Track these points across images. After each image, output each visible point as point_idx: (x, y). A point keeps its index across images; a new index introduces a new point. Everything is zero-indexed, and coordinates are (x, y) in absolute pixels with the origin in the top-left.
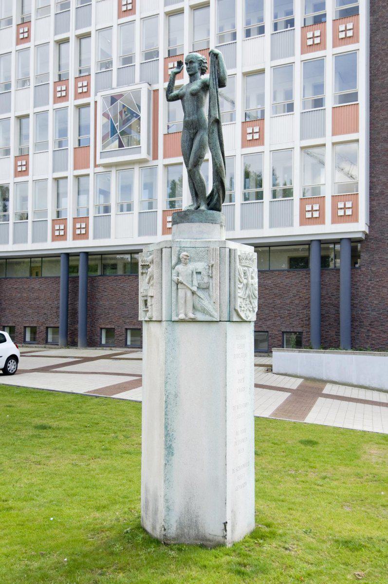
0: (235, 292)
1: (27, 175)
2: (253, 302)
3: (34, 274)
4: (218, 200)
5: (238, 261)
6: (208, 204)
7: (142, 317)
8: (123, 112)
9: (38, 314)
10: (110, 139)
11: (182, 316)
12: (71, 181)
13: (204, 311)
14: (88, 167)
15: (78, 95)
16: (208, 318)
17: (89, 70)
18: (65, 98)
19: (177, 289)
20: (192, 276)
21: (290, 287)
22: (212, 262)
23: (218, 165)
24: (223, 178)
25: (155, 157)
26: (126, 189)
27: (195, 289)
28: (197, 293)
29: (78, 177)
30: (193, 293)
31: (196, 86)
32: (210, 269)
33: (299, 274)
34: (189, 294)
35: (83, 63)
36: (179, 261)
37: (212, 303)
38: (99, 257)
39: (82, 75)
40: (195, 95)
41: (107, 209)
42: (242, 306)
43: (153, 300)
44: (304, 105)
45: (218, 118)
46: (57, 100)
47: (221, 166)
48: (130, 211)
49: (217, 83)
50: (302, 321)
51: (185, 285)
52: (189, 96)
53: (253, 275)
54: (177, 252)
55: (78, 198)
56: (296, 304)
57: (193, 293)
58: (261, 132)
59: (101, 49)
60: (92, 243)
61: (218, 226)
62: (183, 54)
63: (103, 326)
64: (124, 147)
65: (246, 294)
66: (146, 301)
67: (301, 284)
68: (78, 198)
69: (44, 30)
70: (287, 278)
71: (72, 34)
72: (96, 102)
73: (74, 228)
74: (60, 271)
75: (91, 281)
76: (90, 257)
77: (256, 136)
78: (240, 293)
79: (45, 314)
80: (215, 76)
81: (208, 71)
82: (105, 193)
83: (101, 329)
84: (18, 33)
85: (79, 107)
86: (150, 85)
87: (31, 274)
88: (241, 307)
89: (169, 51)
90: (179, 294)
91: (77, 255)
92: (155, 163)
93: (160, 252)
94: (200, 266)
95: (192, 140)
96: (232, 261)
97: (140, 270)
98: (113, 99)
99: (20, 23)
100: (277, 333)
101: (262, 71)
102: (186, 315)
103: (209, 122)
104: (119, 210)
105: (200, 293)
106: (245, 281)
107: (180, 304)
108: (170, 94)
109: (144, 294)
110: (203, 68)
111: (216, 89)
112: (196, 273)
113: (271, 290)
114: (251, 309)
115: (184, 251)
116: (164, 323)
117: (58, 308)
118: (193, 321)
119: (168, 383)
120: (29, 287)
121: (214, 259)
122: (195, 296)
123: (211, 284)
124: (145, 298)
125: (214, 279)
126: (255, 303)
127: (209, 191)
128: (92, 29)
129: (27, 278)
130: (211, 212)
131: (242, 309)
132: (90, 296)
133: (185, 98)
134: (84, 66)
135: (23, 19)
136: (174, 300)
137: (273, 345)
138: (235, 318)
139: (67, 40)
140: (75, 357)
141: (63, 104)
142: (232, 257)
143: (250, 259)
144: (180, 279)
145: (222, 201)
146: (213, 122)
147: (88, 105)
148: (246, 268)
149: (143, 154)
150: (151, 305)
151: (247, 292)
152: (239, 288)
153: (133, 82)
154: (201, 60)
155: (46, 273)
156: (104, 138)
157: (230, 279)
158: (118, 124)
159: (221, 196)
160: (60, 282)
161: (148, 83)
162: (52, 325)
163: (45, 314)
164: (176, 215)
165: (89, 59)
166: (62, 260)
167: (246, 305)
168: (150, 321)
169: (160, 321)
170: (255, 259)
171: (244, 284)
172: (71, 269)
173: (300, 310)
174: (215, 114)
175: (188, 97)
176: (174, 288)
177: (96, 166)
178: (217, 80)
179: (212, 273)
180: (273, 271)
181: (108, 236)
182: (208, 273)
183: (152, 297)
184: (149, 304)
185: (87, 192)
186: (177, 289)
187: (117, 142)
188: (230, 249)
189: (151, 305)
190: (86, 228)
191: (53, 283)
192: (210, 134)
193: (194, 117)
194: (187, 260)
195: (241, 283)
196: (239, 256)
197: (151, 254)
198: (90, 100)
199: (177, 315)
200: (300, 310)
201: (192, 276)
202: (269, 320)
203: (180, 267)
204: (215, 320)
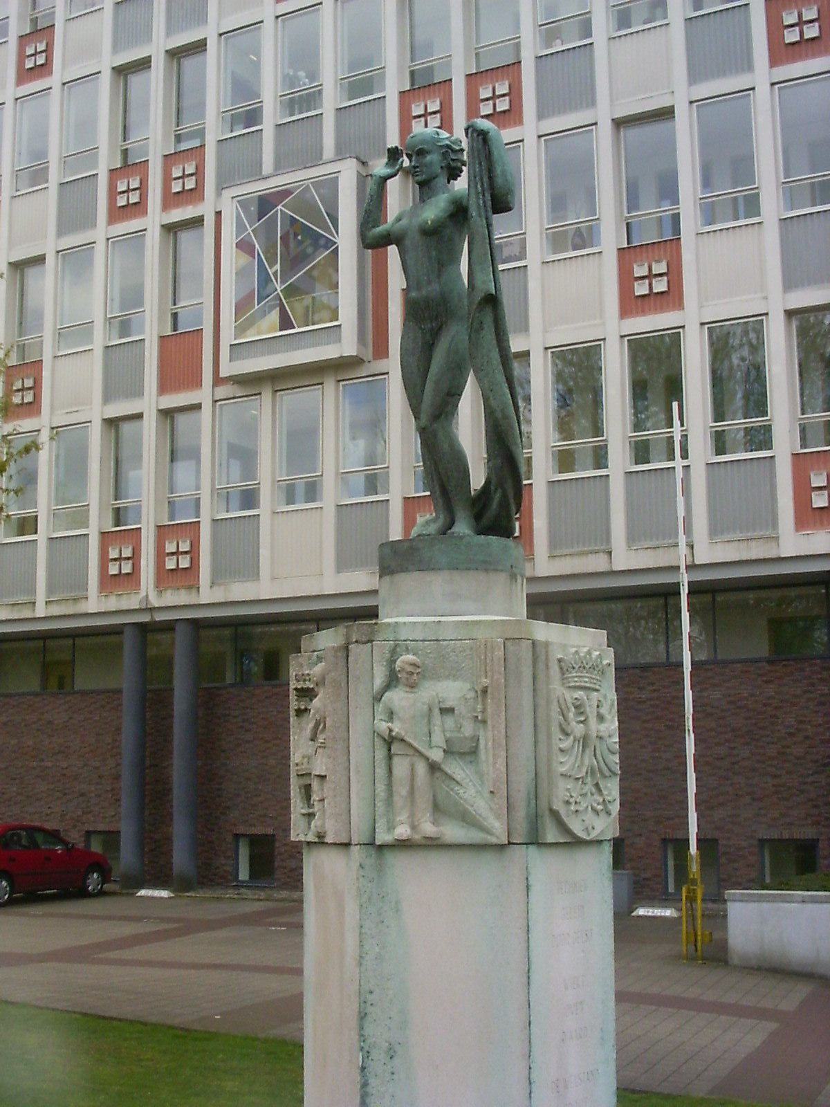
0: (549, 761)
1: (38, 412)
2: (606, 787)
3: (53, 682)
4: (504, 505)
5: (555, 669)
6: (478, 517)
7: (299, 832)
8: (292, 236)
9: (65, 794)
10: (256, 307)
11: (402, 831)
12: (150, 424)
13: (466, 818)
14: (196, 383)
15: (171, 200)
16: (475, 836)
17: (201, 133)
18: (138, 208)
19: (390, 757)
20: (429, 722)
21: (776, 708)
22: (485, 681)
23: (499, 415)
24: (513, 448)
25: (381, 351)
26: (302, 445)
27: (436, 755)
28: (443, 766)
29: (168, 414)
30: (434, 767)
31: (434, 211)
32: (480, 699)
33: (802, 670)
34: (421, 768)
35: (185, 115)
36: (392, 680)
37: (487, 795)
38: (227, 632)
39: (184, 146)
40: (431, 233)
41: (249, 498)
42: (572, 800)
43: (328, 785)
44: (791, 194)
45: (494, 292)
46: (118, 213)
47: (506, 417)
48: (313, 500)
49: (489, 203)
50: (816, 806)
51: (410, 745)
52: (417, 236)
53: (603, 711)
54: (388, 655)
55: (171, 470)
56: (798, 758)
57: (434, 767)
58: (674, 274)
59: (233, 73)
60: (211, 594)
61: (502, 578)
62: (451, 80)
63: (241, 829)
64: (294, 328)
65: (582, 763)
66: (307, 789)
67: (809, 700)
68: (171, 470)
69: (87, 45)
70: (767, 682)
71: (157, 47)
72: (218, 214)
73: (161, 555)
74: (125, 677)
75: (208, 702)
76: (203, 633)
77: (660, 286)
78: (565, 764)
79: (82, 795)
80: (482, 185)
81: (465, 174)
82: (245, 456)
83: (237, 836)
84: (22, 57)
85: (171, 230)
86: (363, 163)
87: (44, 686)
88: (568, 803)
89: (412, 73)
90: (396, 771)
91: (169, 627)
92: (380, 365)
93: (341, 654)
94: (452, 690)
95: (429, 348)
96: (541, 676)
97: (294, 703)
98: (265, 204)
99: (28, 32)
100: (744, 844)
101: (666, 114)
102: (414, 827)
103: (470, 303)
104: (283, 497)
105: (456, 769)
106: (579, 730)
107: (396, 798)
108: (370, 229)
109: (304, 768)
110: (453, 164)
111: (487, 219)
112: (441, 710)
113: (724, 718)
114: (600, 807)
115: (407, 651)
116: (355, 850)
117: (117, 778)
118: (433, 845)
119: (369, 1018)
120: (40, 720)
121: (489, 674)
122: (438, 774)
123: (482, 742)
124: (306, 781)
125: (490, 728)
126: (612, 789)
127: (477, 480)
128: (209, 31)
129: (36, 695)
130: (482, 538)
131: (573, 808)
132: (207, 743)
133: (407, 242)
134: (188, 126)
135: (34, 21)
136: (381, 788)
137: (734, 880)
138: (551, 835)
139: (144, 64)
140: (169, 920)
141: (133, 225)
142: (541, 666)
143: (593, 668)
144: (397, 728)
145: (513, 508)
146: (480, 303)
147: (198, 222)
148: (581, 693)
149: (348, 346)
150: (322, 800)
151: (587, 762)
152: (562, 750)
153: (315, 158)
154: (448, 146)
155: (84, 680)
156: (241, 307)
157: (535, 726)
158: (278, 267)
159: (511, 493)
160: (121, 705)
161: (358, 159)
162: (101, 827)
163: (82, 795)
164: (387, 551)
165: (202, 105)
166: (129, 642)
167: (584, 795)
168: (321, 842)
169: (347, 845)
170: (609, 665)
171: (575, 737)
172: (153, 671)
173: (808, 775)
174: (484, 282)
175: (414, 238)
176: (381, 753)
177: (218, 381)
178: (488, 197)
179: (484, 711)
180: (725, 663)
181: (252, 572)
182: (475, 710)
183: (323, 777)
184: (315, 797)
185: (194, 454)
186: (390, 757)
187: (274, 316)
188: (533, 643)
189: (322, 800)
190: (194, 552)
191: (103, 707)
192: (475, 330)
193: (433, 289)
194: (415, 677)
195: (567, 734)
196: (560, 661)
197: (320, 659)
198: (205, 209)
199: (391, 828)
200: (808, 775)
201: (429, 722)
202: (721, 804)
203: (397, 697)
204: (494, 840)
